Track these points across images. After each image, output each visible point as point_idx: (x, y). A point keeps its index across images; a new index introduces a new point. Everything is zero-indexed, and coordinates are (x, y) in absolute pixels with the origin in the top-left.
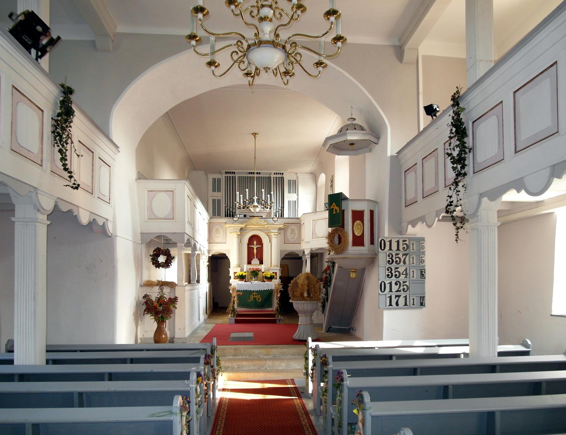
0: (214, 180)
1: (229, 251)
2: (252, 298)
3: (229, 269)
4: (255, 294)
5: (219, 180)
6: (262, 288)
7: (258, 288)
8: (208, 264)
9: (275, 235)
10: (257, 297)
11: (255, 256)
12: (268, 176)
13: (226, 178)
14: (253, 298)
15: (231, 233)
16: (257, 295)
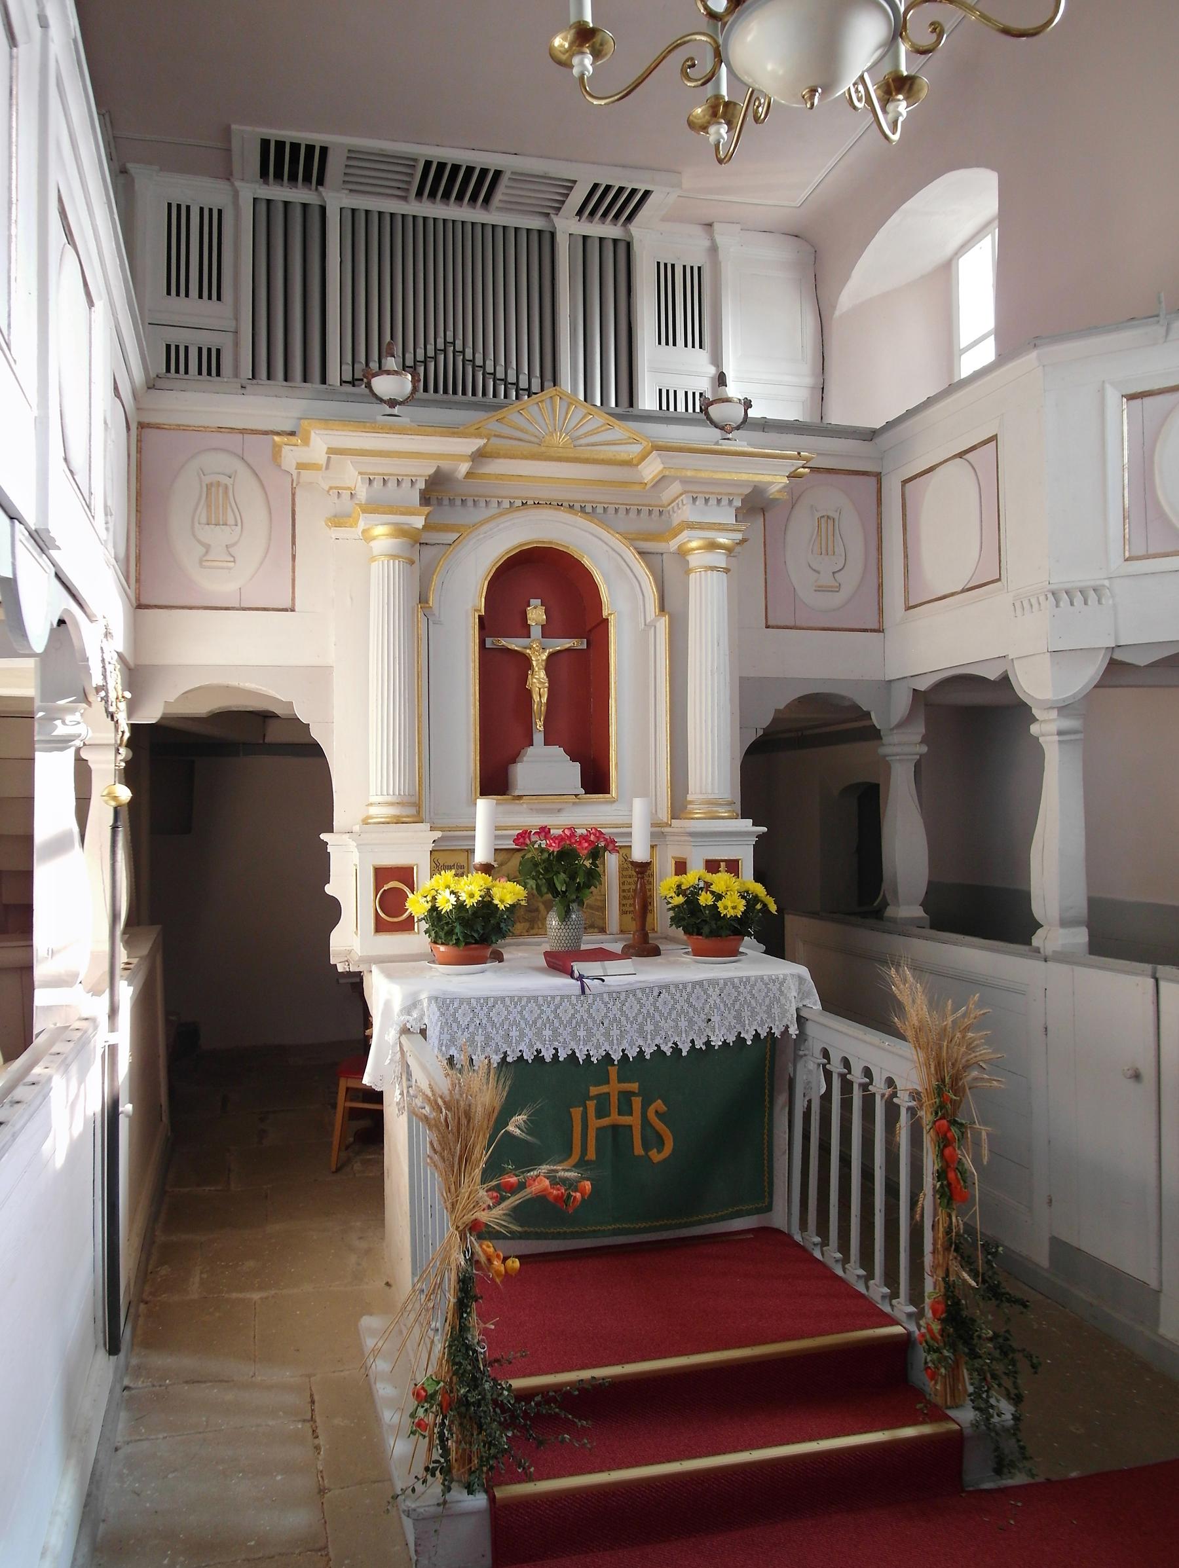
0: (177, 215)
1: (319, 676)
2: (592, 1134)
3: (324, 836)
4: (614, 1087)
5: (213, 220)
6: (683, 1024)
7: (649, 1027)
8: (125, 794)
9: (712, 546)
11: (539, 725)
12: (536, 223)
13: (262, 208)
15: (339, 520)
16: (637, 1102)
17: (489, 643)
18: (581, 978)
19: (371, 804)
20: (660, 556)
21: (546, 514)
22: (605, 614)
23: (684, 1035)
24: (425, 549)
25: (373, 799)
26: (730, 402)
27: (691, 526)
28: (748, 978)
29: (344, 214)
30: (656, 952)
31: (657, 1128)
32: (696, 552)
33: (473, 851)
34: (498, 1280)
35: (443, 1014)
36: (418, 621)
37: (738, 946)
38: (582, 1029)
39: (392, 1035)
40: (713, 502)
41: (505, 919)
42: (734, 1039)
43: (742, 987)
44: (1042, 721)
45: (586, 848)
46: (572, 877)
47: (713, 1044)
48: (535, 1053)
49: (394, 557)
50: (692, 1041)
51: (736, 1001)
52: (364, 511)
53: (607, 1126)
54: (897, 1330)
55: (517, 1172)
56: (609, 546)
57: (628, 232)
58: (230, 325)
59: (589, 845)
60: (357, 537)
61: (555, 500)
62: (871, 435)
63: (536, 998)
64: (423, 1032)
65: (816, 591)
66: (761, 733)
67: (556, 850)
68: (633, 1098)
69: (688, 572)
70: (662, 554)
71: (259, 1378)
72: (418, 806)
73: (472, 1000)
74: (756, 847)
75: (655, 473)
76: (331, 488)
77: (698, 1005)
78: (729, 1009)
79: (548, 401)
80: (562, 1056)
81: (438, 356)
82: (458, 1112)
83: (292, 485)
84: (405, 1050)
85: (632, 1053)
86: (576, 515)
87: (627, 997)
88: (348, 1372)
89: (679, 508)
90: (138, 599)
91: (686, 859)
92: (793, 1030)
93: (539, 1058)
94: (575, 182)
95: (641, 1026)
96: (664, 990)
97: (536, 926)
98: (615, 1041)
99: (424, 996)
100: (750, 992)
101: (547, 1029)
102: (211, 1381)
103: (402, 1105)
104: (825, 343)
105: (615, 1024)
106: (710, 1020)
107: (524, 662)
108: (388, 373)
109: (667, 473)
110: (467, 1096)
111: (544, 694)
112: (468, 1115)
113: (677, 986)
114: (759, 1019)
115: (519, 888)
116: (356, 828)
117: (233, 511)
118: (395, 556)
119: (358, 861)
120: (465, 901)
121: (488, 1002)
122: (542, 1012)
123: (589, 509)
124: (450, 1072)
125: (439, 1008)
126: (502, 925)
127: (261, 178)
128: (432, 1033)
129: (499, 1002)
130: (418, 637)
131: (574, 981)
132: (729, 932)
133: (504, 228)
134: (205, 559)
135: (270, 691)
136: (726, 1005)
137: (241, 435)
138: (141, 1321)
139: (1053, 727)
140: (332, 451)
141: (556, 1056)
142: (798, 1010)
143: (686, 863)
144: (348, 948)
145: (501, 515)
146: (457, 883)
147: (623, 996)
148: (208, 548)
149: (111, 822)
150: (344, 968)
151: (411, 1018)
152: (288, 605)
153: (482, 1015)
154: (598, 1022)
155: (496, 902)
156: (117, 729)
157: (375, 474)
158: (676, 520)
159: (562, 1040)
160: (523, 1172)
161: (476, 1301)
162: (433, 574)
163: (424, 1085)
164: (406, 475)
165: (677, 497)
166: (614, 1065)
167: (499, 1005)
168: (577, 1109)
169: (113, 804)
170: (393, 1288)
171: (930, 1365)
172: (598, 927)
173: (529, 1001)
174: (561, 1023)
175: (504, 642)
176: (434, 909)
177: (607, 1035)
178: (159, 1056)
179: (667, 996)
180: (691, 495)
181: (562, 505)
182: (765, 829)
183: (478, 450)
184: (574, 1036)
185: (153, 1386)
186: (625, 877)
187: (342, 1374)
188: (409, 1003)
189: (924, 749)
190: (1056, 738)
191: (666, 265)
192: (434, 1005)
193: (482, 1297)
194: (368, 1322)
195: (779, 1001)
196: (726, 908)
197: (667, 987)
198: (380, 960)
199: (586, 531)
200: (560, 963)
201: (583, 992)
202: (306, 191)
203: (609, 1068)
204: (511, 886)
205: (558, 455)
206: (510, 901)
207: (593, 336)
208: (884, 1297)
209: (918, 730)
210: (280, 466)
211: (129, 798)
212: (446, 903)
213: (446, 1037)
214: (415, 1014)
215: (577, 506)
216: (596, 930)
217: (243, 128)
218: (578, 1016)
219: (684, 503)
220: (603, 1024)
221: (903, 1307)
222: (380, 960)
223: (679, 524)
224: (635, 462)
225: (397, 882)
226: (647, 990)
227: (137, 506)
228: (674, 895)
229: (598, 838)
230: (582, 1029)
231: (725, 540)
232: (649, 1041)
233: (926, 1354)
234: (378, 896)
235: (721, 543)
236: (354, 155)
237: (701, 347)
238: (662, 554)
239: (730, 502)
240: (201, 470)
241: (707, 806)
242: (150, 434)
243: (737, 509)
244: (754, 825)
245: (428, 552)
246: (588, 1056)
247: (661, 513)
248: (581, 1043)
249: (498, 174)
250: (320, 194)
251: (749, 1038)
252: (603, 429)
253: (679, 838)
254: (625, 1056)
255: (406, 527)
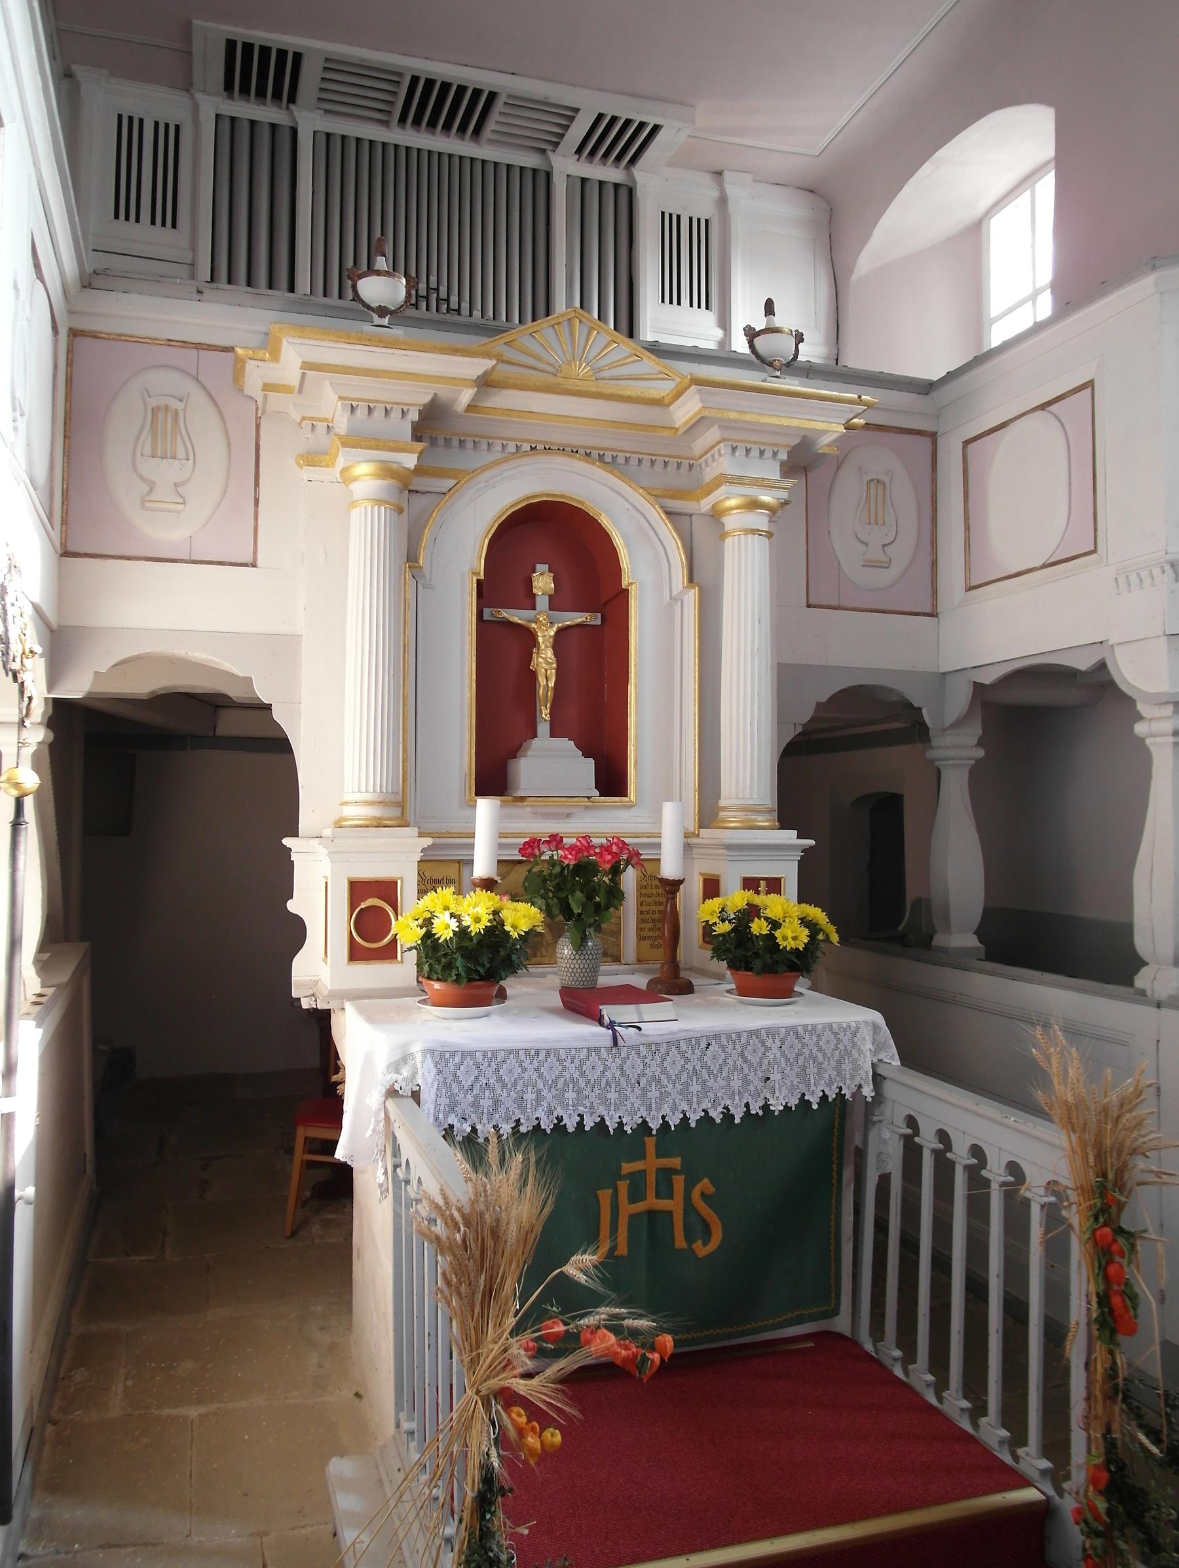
3: (287, 841)
4: (651, 1163)
6: (736, 1083)
7: (695, 1088)
9: (753, 505)
10: (675, 1205)
11: (545, 713)
12: (530, 160)
13: (226, 126)
14: (633, 1217)
15: (312, 459)
16: (679, 1182)
17: (487, 614)
18: (611, 1026)
19: (346, 803)
20: (687, 518)
21: (559, 462)
22: (624, 584)
23: (737, 1098)
24: (416, 498)
25: (348, 797)
26: (781, 332)
27: (730, 480)
28: (814, 1027)
29: (317, 138)
30: (687, 989)
31: (703, 1213)
32: (735, 511)
33: (471, 862)
34: (532, 1462)
35: (440, 1072)
36: (405, 583)
37: (794, 984)
38: (613, 1090)
39: (375, 1098)
40: (755, 453)
41: (517, 949)
42: (797, 1102)
43: (807, 1037)
44: (1151, 719)
45: (608, 862)
46: (590, 897)
47: (772, 1108)
48: (556, 1121)
49: (379, 502)
50: (747, 1105)
51: (800, 1053)
52: (345, 445)
53: (642, 1212)
54: (1030, 1495)
55: (564, 1318)
56: (631, 503)
57: (631, 176)
58: (187, 256)
59: (613, 857)
60: (334, 479)
61: (568, 446)
62: (926, 388)
63: (556, 1052)
64: (416, 1096)
65: (863, 566)
66: (799, 729)
67: (573, 863)
68: (673, 1177)
69: (723, 535)
70: (691, 515)
71: (197, 1539)
72: (401, 805)
73: (478, 1054)
74: (801, 863)
75: (691, 414)
76: (304, 418)
77: (754, 1060)
78: (791, 1065)
79: (566, 323)
80: (589, 1124)
81: (419, 302)
82: (483, 1230)
83: (257, 414)
84: (392, 1119)
85: (674, 1120)
86: (594, 464)
87: (669, 1049)
88: (310, 1529)
89: (714, 460)
90: (64, 544)
91: (718, 876)
92: (868, 1091)
93: (559, 1127)
94: (577, 110)
95: (686, 1087)
96: (714, 1042)
97: (538, 954)
98: (654, 1106)
99: (416, 1049)
100: (817, 1044)
101: (571, 1091)
102: (135, 1545)
103: (385, 1187)
104: (840, 311)
105: (653, 1084)
106: (768, 1079)
107: (527, 638)
108: (379, 273)
109: (706, 414)
110: (494, 1208)
111: (551, 677)
112: (495, 1233)
113: (729, 1036)
114: (827, 1077)
115: (534, 910)
116: (328, 832)
117: (183, 441)
118: (380, 501)
119: (330, 872)
120: (469, 927)
121: (497, 1057)
122: (565, 1068)
123: (608, 459)
124: (473, 1176)
125: (436, 1064)
126: (514, 957)
127: (225, 90)
128: (428, 1096)
129: (511, 1056)
130: (405, 603)
131: (603, 1030)
132: (786, 968)
133: (496, 164)
134: (147, 499)
135: (225, 663)
136: (787, 1060)
137: (195, 351)
138: (47, 1450)
139: (1168, 726)
140: (307, 366)
141: (580, 1124)
142: (873, 1065)
143: (719, 880)
144: (314, 978)
145: (506, 460)
146: (457, 903)
147: (664, 1049)
148: (152, 485)
149: (11, 817)
150: (310, 1004)
151: (400, 1078)
152: (249, 559)
153: (489, 1073)
154: (633, 1082)
155: (508, 928)
156: (22, 692)
157: (358, 400)
158: (709, 474)
159: (588, 1105)
160: (574, 1318)
161: (503, 1495)
162: (425, 528)
163: (432, 1188)
164: (397, 403)
165: (713, 447)
166: (653, 1135)
167: (511, 1061)
168: (606, 1191)
169: (15, 793)
170: (365, 1400)
171: (1090, 1552)
172: (612, 956)
173: (548, 1055)
174: (587, 1082)
175: (505, 614)
176: (429, 935)
177: (644, 1097)
178: (84, 1097)
179: (717, 1049)
180: (729, 443)
181: (577, 452)
182: (812, 842)
183: (485, 374)
184: (604, 1100)
185: (58, 1552)
186: (644, 896)
187: (303, 1531)
188: (399, 1057)
189: (981, 753)
190: (1171, 739)
191: (671, 215)
192: (429, 1062)
193: (511, 1490)
194: (340, 1467)
195: (850, 1055)
196: (785, 938)
197: (717, 1037)
198: (356, 996)
199: (604, 485)
200: (584, 1005)
201: (615, 1043)
202: (275, 109)
203: (646, 1139)
204: (523, 907)
205: (578, 388)
206: (524, 927)
207: (590, 291)
208: (1001, 1442)
209: (975, 731)
210: (241, 390)
211: (37, 786)
212: (444, 929)
213: (444, 1101)
214: (405, 1072)
215: (595, 454)
216: (609, 959)
217: (205, 24)
218: (609, 1074)
219: (722, 452)
220: (639, 1083)
221: (1033, 1460)
222: (356, 996)
223: (715, 478)
224: (666, 401)
225: (376, 899)
226: (693, 1041)
227: (65, 431)
228: (718, 921)
229: (621, 849)
230: (613, 1090)
231: (769, 498)
232: (695, 1105)
233: (1083, 1538)
234: (354, 916)
235: (765, 503)
236: (332, 65)
237: (707, 308)
238: (691, 515)
239: (775, 454)
240: (147, 391)
241: (744, 813)
242: (83, 343)
243: (782, 464)
244: (798, 837)
245: (420, 502)
246: (621, 1124)
247: (691, 466)
248: (612, 1108)
249: (492, 96)
250: (291, 114)
251: (814, 1100)
252: (629, 360)
253: (710, 851)
254: (665, 1124)
255: (395, 466)
